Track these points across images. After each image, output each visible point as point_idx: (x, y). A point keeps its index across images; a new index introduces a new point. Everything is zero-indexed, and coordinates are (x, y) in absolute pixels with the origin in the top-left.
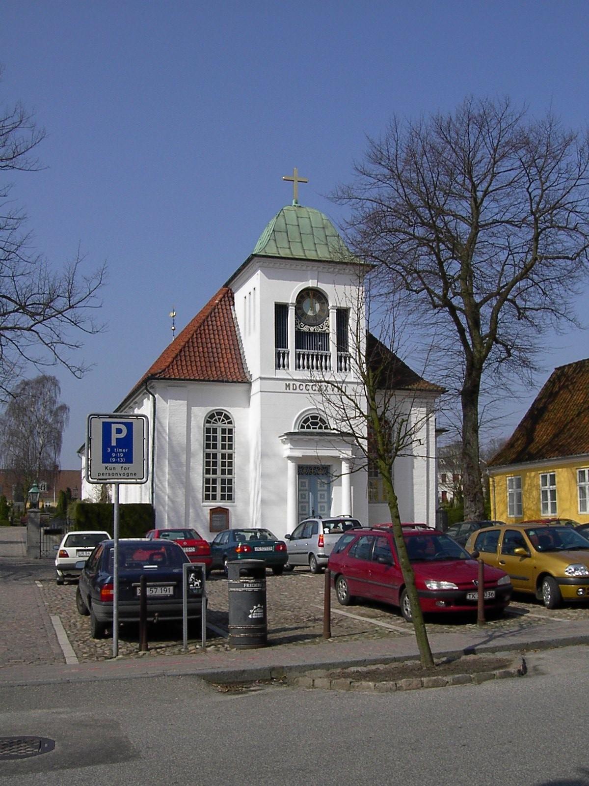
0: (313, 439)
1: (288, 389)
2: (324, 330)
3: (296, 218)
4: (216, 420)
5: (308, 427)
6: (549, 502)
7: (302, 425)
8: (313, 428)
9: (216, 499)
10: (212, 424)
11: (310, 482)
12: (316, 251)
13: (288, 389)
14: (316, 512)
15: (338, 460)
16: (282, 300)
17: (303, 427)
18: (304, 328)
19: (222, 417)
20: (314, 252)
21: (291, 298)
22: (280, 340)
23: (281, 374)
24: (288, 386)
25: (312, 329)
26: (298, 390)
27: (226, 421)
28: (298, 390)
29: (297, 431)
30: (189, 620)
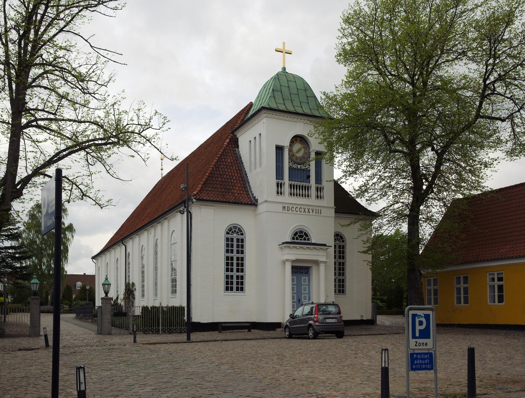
0: (309, 247)
1: (284, 210)
2: (306, 167)
3: (286, 81)
4: (235, 231)
5: (297, 239)
6: (432, 297)
7: (293, 237)
8: (300, 240)
9: (233, 290)
10: (230, 235)
11: (297, 279)
12: (301, 107)
13: (284, 210)
14: (300, 301)
15: (317, 263)
16: (280, 144)
17: (293, 238)
18: (294, 166)
19: (237, 230)
20: (300, 108)
21: (286, 143)
22: (279, 174)
23: (280, 198)
24: (284, 208)
25: (299, 167)
26: (290, 211)
27: (239, 233)
28: (290, 211)
29: (290, 241)
30: (464, 297)
